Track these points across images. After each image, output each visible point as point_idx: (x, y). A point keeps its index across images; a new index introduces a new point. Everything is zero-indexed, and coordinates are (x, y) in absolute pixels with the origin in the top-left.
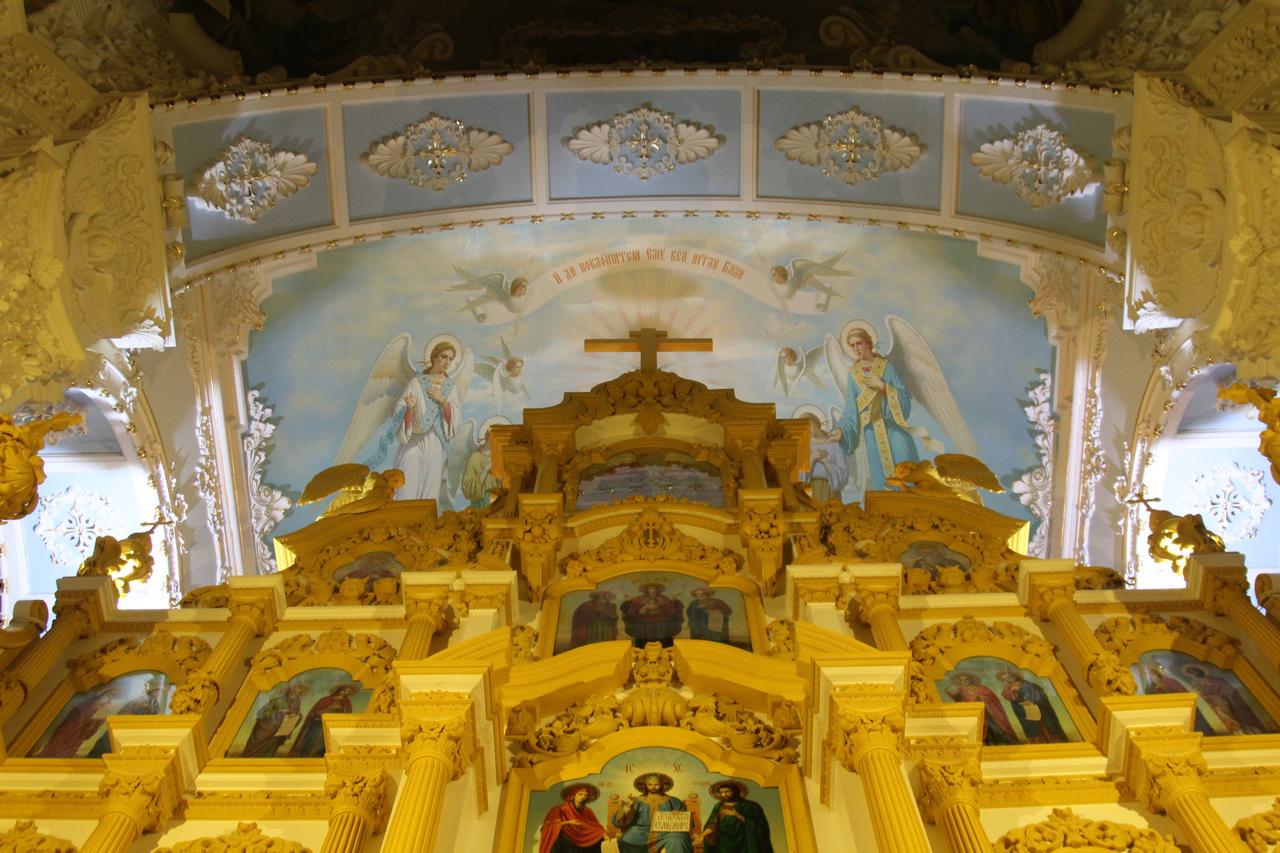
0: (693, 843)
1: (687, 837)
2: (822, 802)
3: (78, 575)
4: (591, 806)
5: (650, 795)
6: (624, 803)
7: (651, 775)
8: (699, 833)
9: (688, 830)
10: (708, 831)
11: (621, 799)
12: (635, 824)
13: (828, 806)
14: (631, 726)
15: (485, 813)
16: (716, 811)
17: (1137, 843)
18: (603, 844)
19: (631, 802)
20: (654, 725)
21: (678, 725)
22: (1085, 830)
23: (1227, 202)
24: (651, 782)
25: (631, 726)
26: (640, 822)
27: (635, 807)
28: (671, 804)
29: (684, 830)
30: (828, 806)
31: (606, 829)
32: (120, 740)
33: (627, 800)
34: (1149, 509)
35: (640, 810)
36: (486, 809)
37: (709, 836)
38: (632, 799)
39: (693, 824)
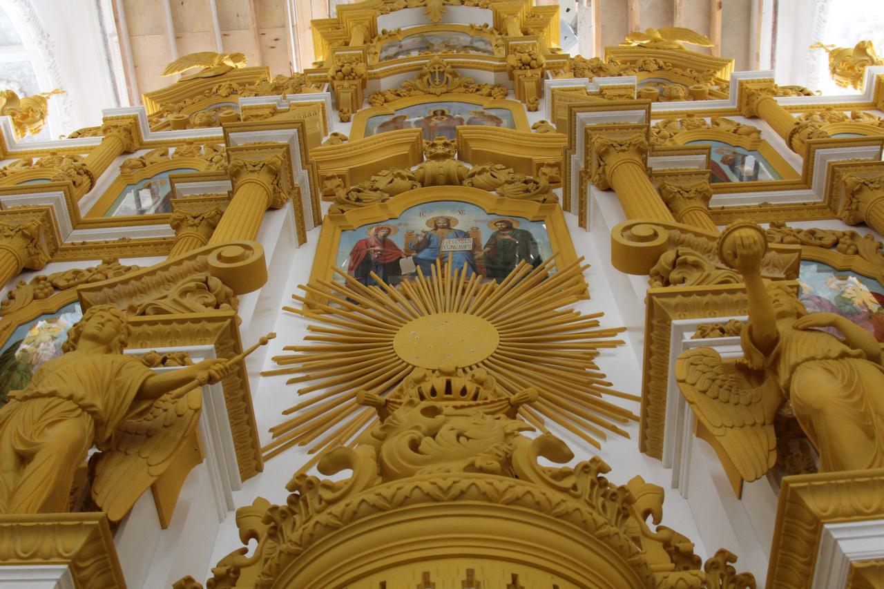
0: (476, 257)
1: (471, 254)
2: (581, 225)
3: (217, 566)
4: (390, 238)
5: (439, 230)
6: (418, 235)
7: (440, 217)
8: (480, 250)
9: (471, 249)
10: (487, 249)
11: (415, 233)
12: (428, 247)
13: (585, 228)
14: (423, 186)
15: (304, 245)
16: (493, 237)
17: (841, 240)
18: (401, 261)
19: (424, 234)
20: (442, 185)
21: (461, 184)
22: (798, 235)
23: (699, 393)
24: (440, 222)
25: (423, 186)
26: (432, 245)
27: (427, 237)
28: (456, 234)
29: (467, 249)
30: (585, 228)
31: (403, 251)
32: (6, 204)
33: (420, 233)
34: (827, 51)
35: (431, 238)
36: (305, 241)
37: (488, 252)
38: (425, 232)
39: (474, 245)
